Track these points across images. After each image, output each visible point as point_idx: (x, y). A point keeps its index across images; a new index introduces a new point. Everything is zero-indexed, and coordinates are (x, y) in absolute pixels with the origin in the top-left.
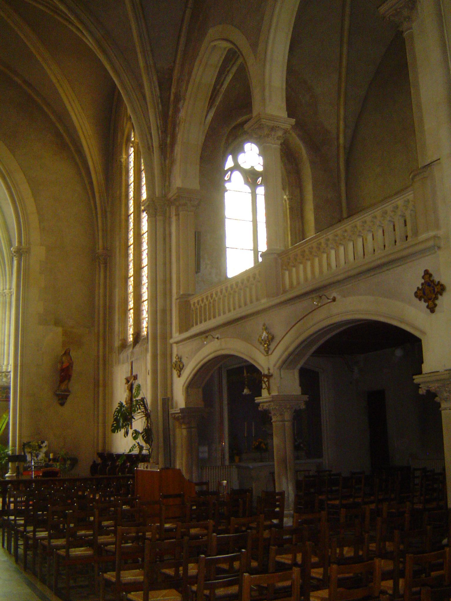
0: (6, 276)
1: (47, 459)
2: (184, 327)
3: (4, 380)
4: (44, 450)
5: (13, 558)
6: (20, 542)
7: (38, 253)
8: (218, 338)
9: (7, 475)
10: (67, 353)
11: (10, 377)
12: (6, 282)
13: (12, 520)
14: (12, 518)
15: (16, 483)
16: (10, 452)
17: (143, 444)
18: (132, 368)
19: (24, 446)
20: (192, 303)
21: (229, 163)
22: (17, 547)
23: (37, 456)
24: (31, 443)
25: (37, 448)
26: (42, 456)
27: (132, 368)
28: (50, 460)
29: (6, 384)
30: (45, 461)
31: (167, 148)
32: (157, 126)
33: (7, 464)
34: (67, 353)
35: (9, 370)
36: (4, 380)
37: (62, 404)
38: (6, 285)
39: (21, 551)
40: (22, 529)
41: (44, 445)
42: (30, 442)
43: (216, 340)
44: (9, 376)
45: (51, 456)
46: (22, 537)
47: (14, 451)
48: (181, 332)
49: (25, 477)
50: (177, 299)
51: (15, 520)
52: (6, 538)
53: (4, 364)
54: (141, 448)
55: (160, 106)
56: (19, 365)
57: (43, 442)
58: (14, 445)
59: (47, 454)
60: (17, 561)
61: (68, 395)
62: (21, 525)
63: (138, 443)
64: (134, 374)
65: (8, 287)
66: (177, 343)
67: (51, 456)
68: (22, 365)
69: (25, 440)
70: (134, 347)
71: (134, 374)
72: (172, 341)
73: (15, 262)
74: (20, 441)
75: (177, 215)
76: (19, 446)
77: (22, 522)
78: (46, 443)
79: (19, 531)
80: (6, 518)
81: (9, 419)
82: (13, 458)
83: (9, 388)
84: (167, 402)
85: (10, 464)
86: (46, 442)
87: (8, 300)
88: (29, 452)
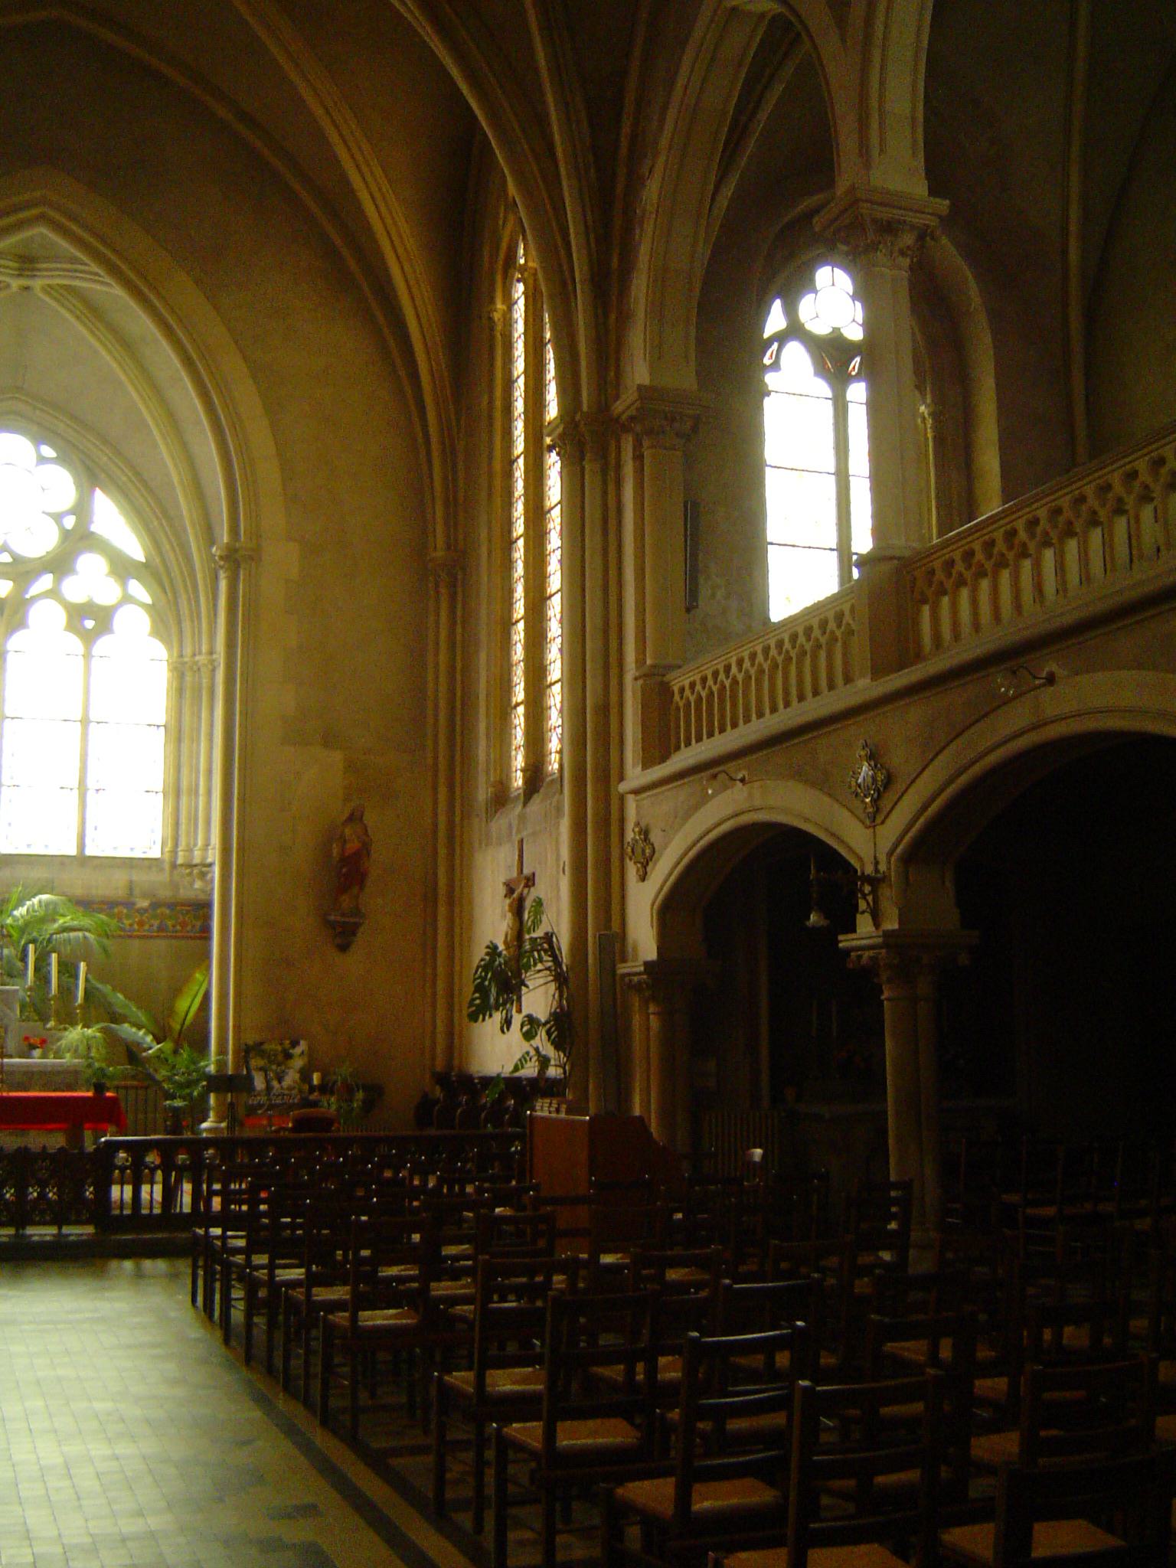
2: (658, 748)
4: (298, 1063)
9: (204, 1125)
17: (549, 1051)
18: (521, 856)
19: (246, 1052)
20: (676, 689)
21: (111, 519)
26: (291, 1078)
27: (521, 856)
28: (312, 1089)
31: (608, 286)
32: (586, 227)
37: (344, 948)
41: (297, 1051)
45: (316, 1078)
48: (647, 763)
57: (295, 1044)
58: (222, 1050)
59: (305, 1075)
64: (526, 871)
66: (636, 792)
67: (316, 1078)
70: (525, 804)
72: (623, 787)
75: (639, 458)
78: (303, 1045)
86: (302, 1042)
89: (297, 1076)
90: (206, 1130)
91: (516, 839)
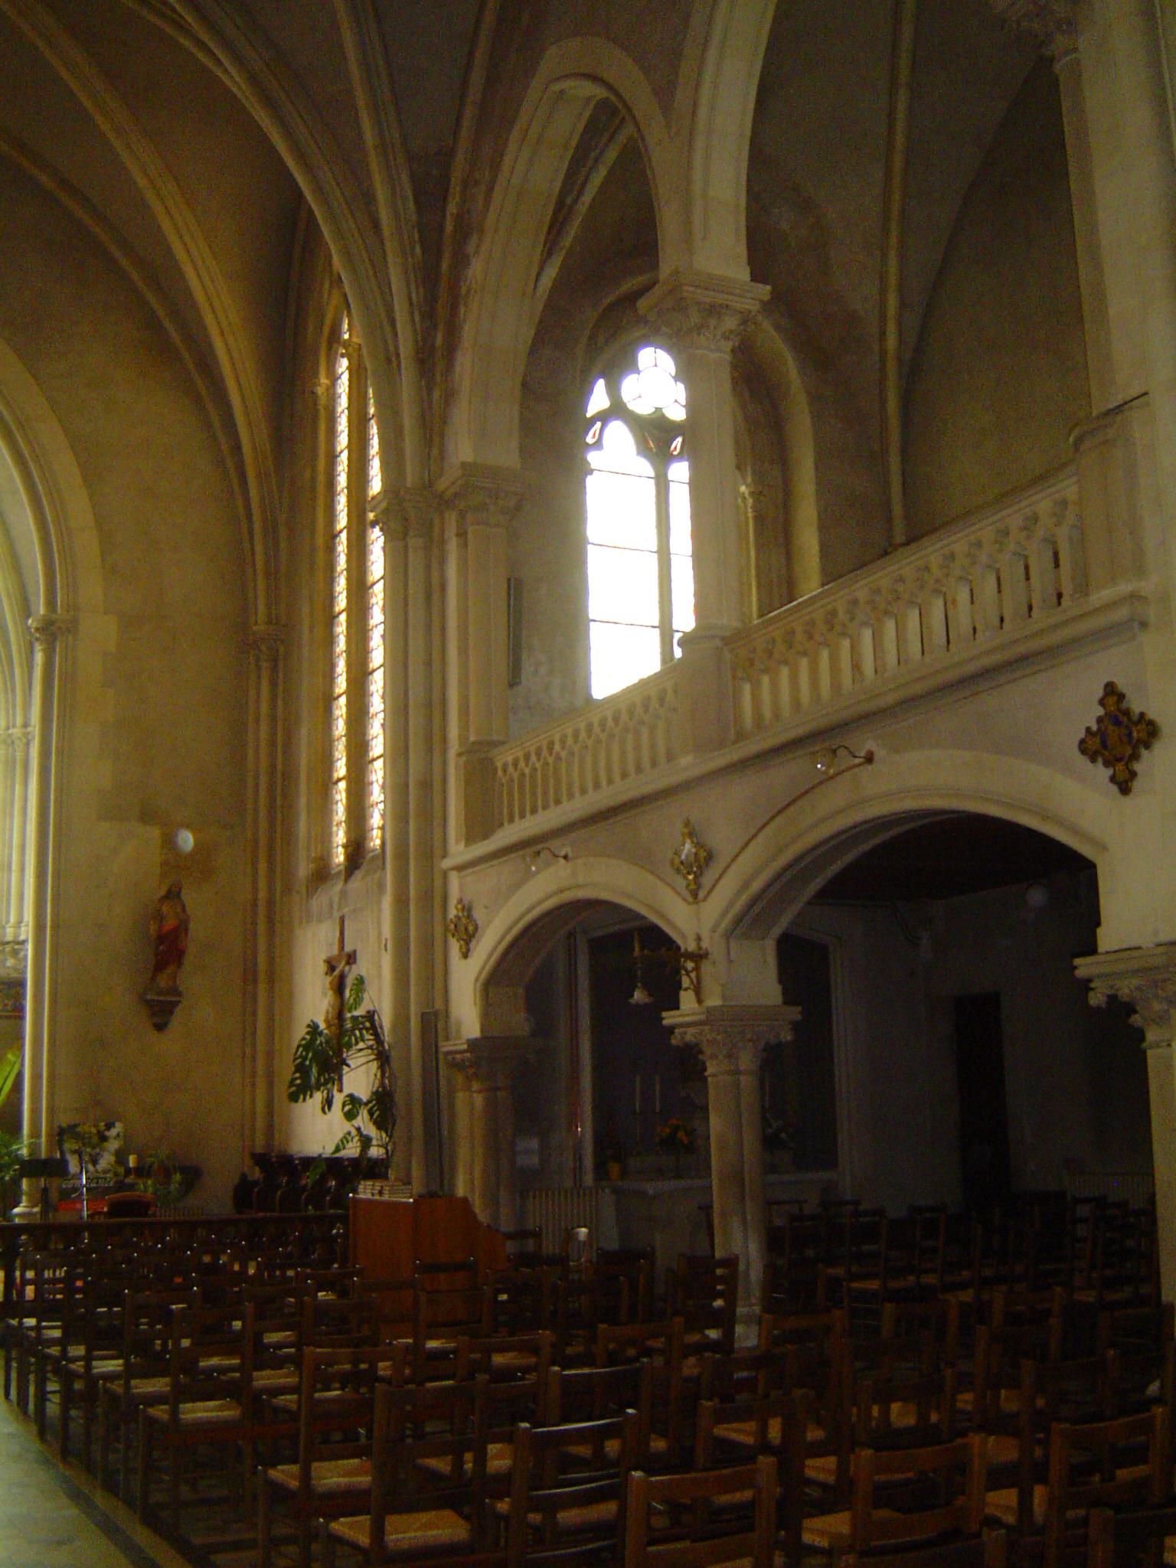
0: (13, 690)
1: (121, 1170)
2: (479, 826)
3: (10, 962)
4: (113, 1145)
5: (34, 1428)
6: (52, 1386)
7: (100, 631)
8: (565, 857)
9: (17, 1210)
10: (173, 895)
11: (26, 956)
12: (14, 707)
13: (31, 1328)
14: (31, 1322)
15: (40, 1232)
16: (25, 1152)
17: (371, 1130)
18: (342, 933)
19: (60, 1135)
20: (499, 764)
21: (598, 400)
22: (42, 1396)
23: (95, 1162)
24: (79, 1129)
25: (95, 1140)
26: (106, 1161)
27: (342, 933)
28: (128, 1171)
29: (14, 975)
30: (116, 1174)
32: (411, 304)
33: (16, 1182)
34: (173, 895)
35: (22, 937)
36: (10, 962)
37: (160, 1027)
38: (14, 714)
39: (53, 1407)
40: (55, 1351)
41: (113, 1132)
42: (75, 1126)
43: (562, 861)
44: (22, 954)
45: (132, 1161)
46: (55, 1372)
47: (34, 1148)
48: (470, 839)
49: (64, 1217)
50: (459, 755)
51: (38, 1328)
52: (14, 1375)
53: (8, 922)
54: (366, 1142)
55: (418, 250)
56: (49, 924)
57: (109, 1126)
58: (35, 1133)
59: (121, 1157)
60: (42, 1434)
61: (177, 1003)
62: (53, 1342)
63: (358, 1129)
64: (348, 948)
65: (19, 720)
66: (460, 868)
67: (132, 1161)
68: (56, 926)
69: (64, 1121)
71: (348, 948)
72: (446, 864)
73: (39, 658)
74: (50, 1122)
75: (462, 534)
76: (48, 1135)
77: (57, 1333)
78: (118, 1128)
79: (48, 1357)
80: (14, 1322)
81: (22, 1065)
82: (34, 1167)
83: (22, 984)
84: (434, 1022)
85: (25, 1184)
87: (19, 755)
88: (75, 1152)
89: (113, 1159)
90: (18, 1215)
91: (336, 915)
